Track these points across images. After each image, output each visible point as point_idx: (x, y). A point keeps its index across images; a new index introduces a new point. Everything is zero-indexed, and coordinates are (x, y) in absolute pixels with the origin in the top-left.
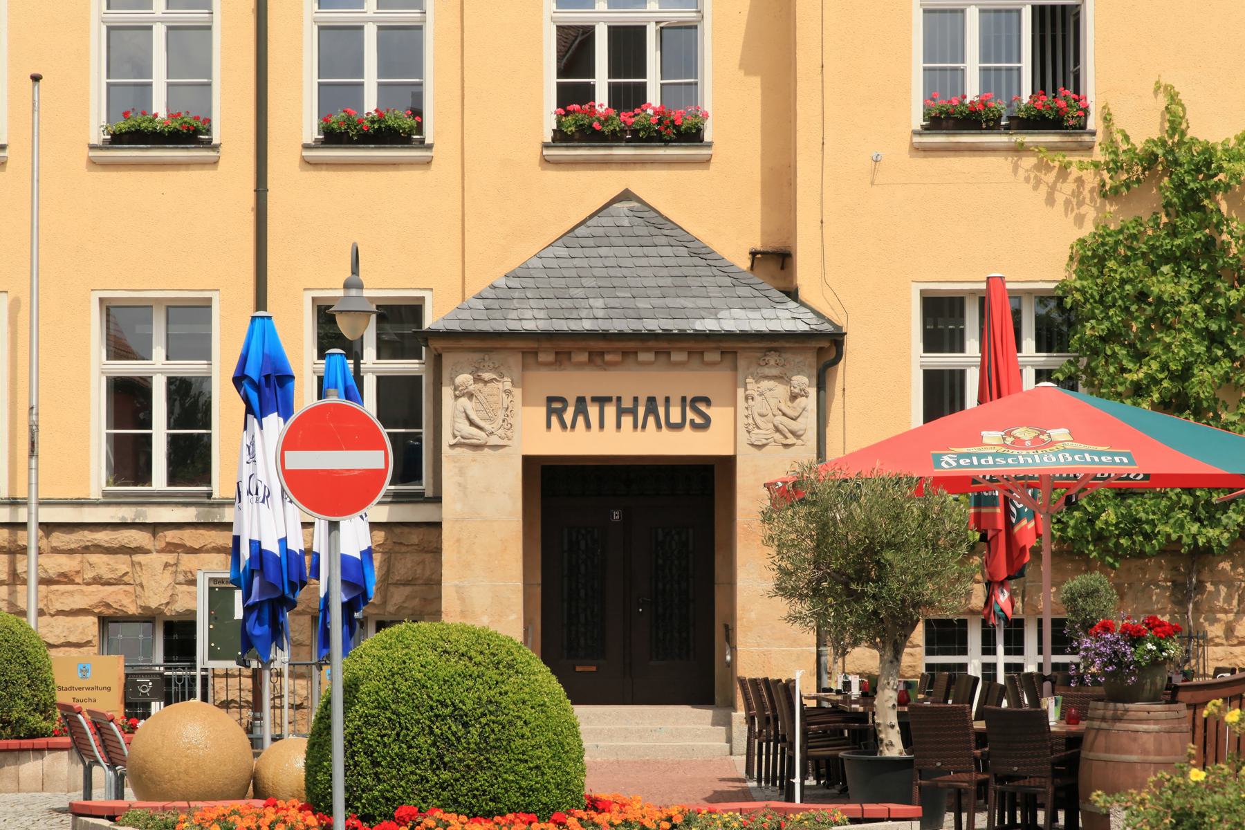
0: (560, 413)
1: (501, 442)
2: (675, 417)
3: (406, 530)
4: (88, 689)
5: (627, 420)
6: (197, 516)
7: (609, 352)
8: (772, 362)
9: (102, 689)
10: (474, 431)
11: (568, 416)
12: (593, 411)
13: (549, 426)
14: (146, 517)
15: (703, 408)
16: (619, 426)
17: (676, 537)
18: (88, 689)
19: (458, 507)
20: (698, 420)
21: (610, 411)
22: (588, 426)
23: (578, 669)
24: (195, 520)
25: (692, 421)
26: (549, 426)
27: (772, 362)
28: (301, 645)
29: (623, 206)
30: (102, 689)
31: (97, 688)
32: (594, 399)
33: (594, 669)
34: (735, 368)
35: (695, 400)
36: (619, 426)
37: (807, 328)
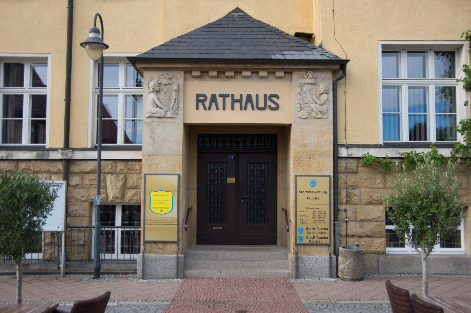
0: (203, 102)
1: (173, 116)
2: (261, 105)
3: (134, 163)
4: (315, 192)
5: (237, 105)
6: (36, 156)
7: (227, 71)
8: (310, 76)
9: (323, 192)
10: (158, 110)
11: (207, 104)
12: (220, 100)
13: (197, 108)
14: (13, 156)
15: (275, 99)
16: (233, 109)
17: (259, 168)
18: (315, 192)
19: (150, 148)
20: (273, 106)
21: (229, 100)
22: (217, 108)
23: (214, 228)
24: (35, 158)
25: (270, 106)
26: (197, 108)
27: (310, 76)
28: (84, 216)
29: (236, 14)
30: (323, 192)
31: (319, 192)
32: (220, 95)
33: (221, 228)
34: (291, 80)
35: (271, 96)
36: (233, 109)
37: (328, 59)
